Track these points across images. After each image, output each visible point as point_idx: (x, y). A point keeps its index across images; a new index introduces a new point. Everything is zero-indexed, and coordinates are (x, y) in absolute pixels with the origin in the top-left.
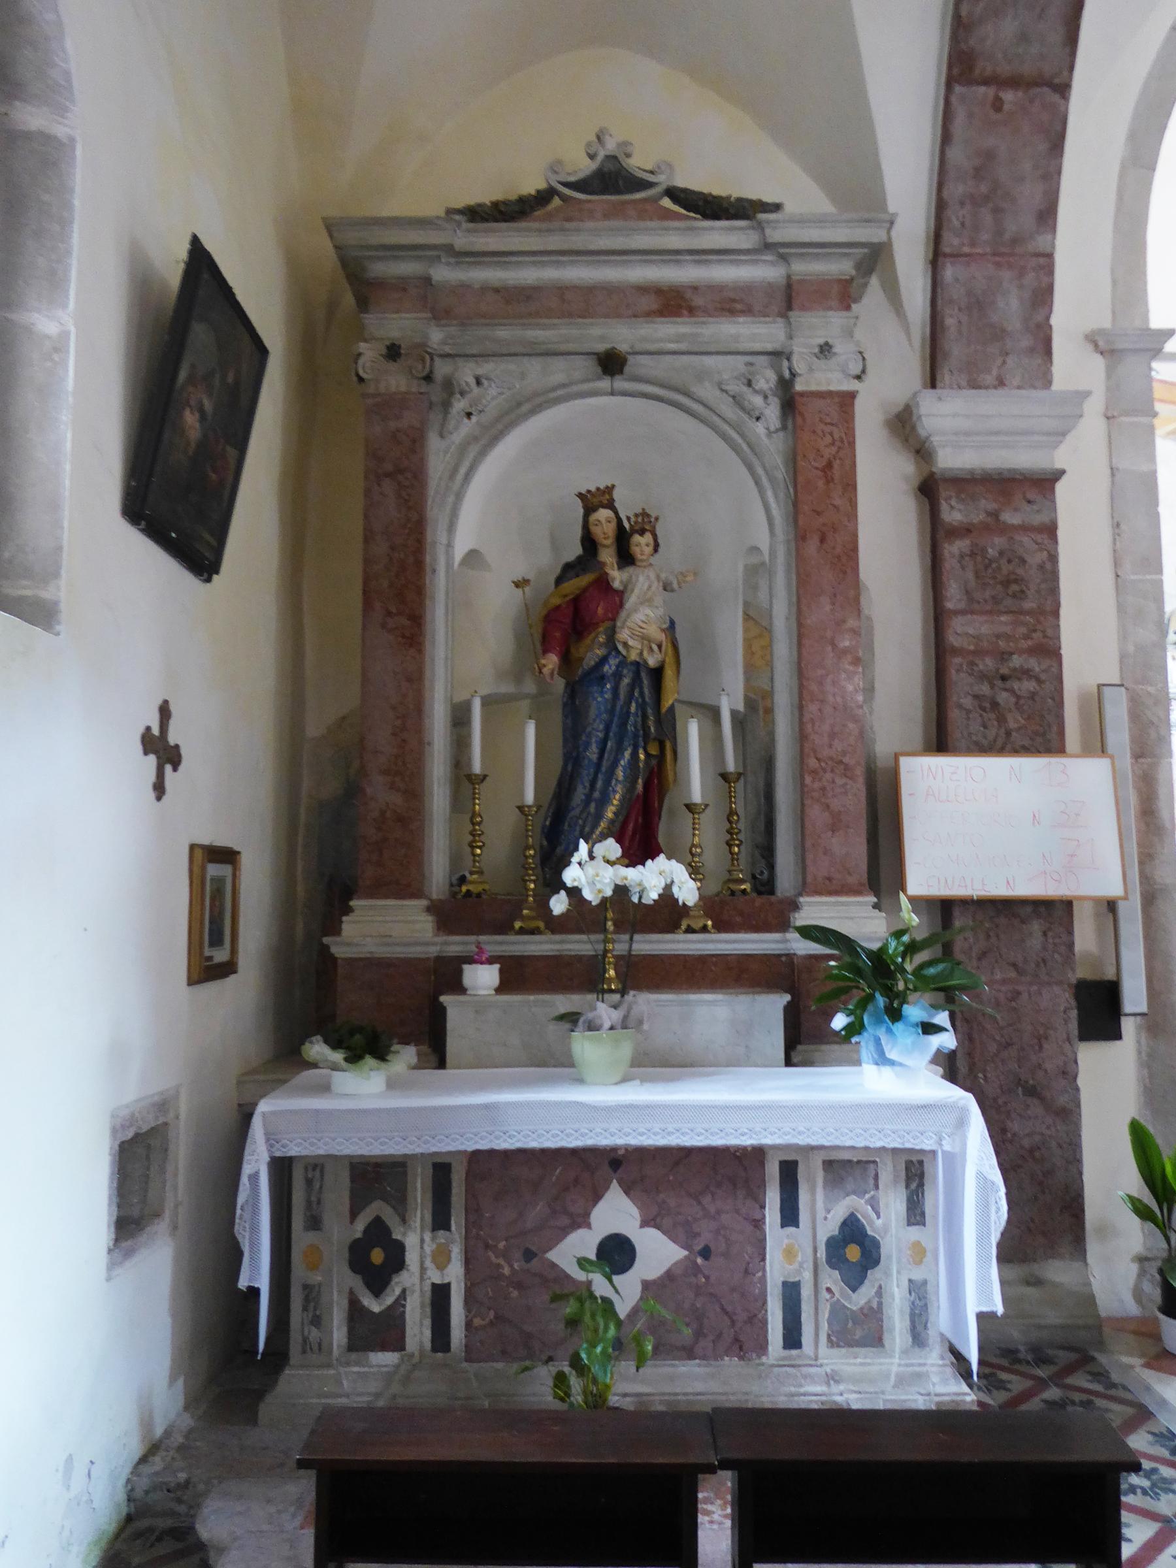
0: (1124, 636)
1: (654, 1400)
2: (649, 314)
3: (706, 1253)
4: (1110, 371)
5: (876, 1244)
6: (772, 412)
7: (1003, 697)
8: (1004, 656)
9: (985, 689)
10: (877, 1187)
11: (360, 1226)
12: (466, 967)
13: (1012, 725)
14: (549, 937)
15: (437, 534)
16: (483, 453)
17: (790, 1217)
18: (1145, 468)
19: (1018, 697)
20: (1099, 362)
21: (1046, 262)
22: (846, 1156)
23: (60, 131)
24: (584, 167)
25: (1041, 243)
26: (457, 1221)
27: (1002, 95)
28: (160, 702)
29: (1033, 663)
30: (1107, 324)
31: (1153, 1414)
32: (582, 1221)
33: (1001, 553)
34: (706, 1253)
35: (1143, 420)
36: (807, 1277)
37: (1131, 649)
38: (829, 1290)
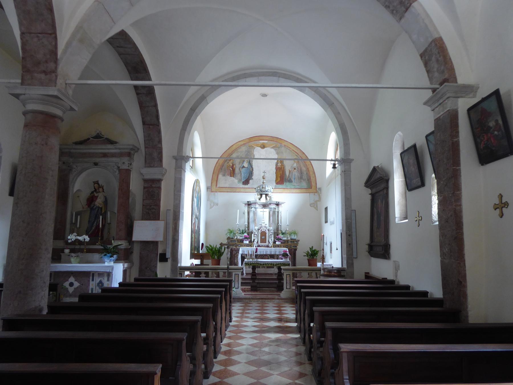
0: (174, 202)
2: (102, 157)
3: (82, 284)
4: (176, 162)
5: (103, 284)
6: (117, 172)
8: (151, 206)
9: (147, 211)
10: (104, 277)
12: (65, 250)
13: (151, 216)
17: (93, 280)
18: (180, 177)
19: (152, 212)
20: (174, 161)
21: (161, 149)
22: (101, 273)
24: (94, 134)
25: (159, 145)
27: (150, 126)
30: (176, 155)
31: (253, 351)
32: (68, 280)
34: (82, 284)
36: (94, 288)
37: (175, 204)
38: (97, 289)
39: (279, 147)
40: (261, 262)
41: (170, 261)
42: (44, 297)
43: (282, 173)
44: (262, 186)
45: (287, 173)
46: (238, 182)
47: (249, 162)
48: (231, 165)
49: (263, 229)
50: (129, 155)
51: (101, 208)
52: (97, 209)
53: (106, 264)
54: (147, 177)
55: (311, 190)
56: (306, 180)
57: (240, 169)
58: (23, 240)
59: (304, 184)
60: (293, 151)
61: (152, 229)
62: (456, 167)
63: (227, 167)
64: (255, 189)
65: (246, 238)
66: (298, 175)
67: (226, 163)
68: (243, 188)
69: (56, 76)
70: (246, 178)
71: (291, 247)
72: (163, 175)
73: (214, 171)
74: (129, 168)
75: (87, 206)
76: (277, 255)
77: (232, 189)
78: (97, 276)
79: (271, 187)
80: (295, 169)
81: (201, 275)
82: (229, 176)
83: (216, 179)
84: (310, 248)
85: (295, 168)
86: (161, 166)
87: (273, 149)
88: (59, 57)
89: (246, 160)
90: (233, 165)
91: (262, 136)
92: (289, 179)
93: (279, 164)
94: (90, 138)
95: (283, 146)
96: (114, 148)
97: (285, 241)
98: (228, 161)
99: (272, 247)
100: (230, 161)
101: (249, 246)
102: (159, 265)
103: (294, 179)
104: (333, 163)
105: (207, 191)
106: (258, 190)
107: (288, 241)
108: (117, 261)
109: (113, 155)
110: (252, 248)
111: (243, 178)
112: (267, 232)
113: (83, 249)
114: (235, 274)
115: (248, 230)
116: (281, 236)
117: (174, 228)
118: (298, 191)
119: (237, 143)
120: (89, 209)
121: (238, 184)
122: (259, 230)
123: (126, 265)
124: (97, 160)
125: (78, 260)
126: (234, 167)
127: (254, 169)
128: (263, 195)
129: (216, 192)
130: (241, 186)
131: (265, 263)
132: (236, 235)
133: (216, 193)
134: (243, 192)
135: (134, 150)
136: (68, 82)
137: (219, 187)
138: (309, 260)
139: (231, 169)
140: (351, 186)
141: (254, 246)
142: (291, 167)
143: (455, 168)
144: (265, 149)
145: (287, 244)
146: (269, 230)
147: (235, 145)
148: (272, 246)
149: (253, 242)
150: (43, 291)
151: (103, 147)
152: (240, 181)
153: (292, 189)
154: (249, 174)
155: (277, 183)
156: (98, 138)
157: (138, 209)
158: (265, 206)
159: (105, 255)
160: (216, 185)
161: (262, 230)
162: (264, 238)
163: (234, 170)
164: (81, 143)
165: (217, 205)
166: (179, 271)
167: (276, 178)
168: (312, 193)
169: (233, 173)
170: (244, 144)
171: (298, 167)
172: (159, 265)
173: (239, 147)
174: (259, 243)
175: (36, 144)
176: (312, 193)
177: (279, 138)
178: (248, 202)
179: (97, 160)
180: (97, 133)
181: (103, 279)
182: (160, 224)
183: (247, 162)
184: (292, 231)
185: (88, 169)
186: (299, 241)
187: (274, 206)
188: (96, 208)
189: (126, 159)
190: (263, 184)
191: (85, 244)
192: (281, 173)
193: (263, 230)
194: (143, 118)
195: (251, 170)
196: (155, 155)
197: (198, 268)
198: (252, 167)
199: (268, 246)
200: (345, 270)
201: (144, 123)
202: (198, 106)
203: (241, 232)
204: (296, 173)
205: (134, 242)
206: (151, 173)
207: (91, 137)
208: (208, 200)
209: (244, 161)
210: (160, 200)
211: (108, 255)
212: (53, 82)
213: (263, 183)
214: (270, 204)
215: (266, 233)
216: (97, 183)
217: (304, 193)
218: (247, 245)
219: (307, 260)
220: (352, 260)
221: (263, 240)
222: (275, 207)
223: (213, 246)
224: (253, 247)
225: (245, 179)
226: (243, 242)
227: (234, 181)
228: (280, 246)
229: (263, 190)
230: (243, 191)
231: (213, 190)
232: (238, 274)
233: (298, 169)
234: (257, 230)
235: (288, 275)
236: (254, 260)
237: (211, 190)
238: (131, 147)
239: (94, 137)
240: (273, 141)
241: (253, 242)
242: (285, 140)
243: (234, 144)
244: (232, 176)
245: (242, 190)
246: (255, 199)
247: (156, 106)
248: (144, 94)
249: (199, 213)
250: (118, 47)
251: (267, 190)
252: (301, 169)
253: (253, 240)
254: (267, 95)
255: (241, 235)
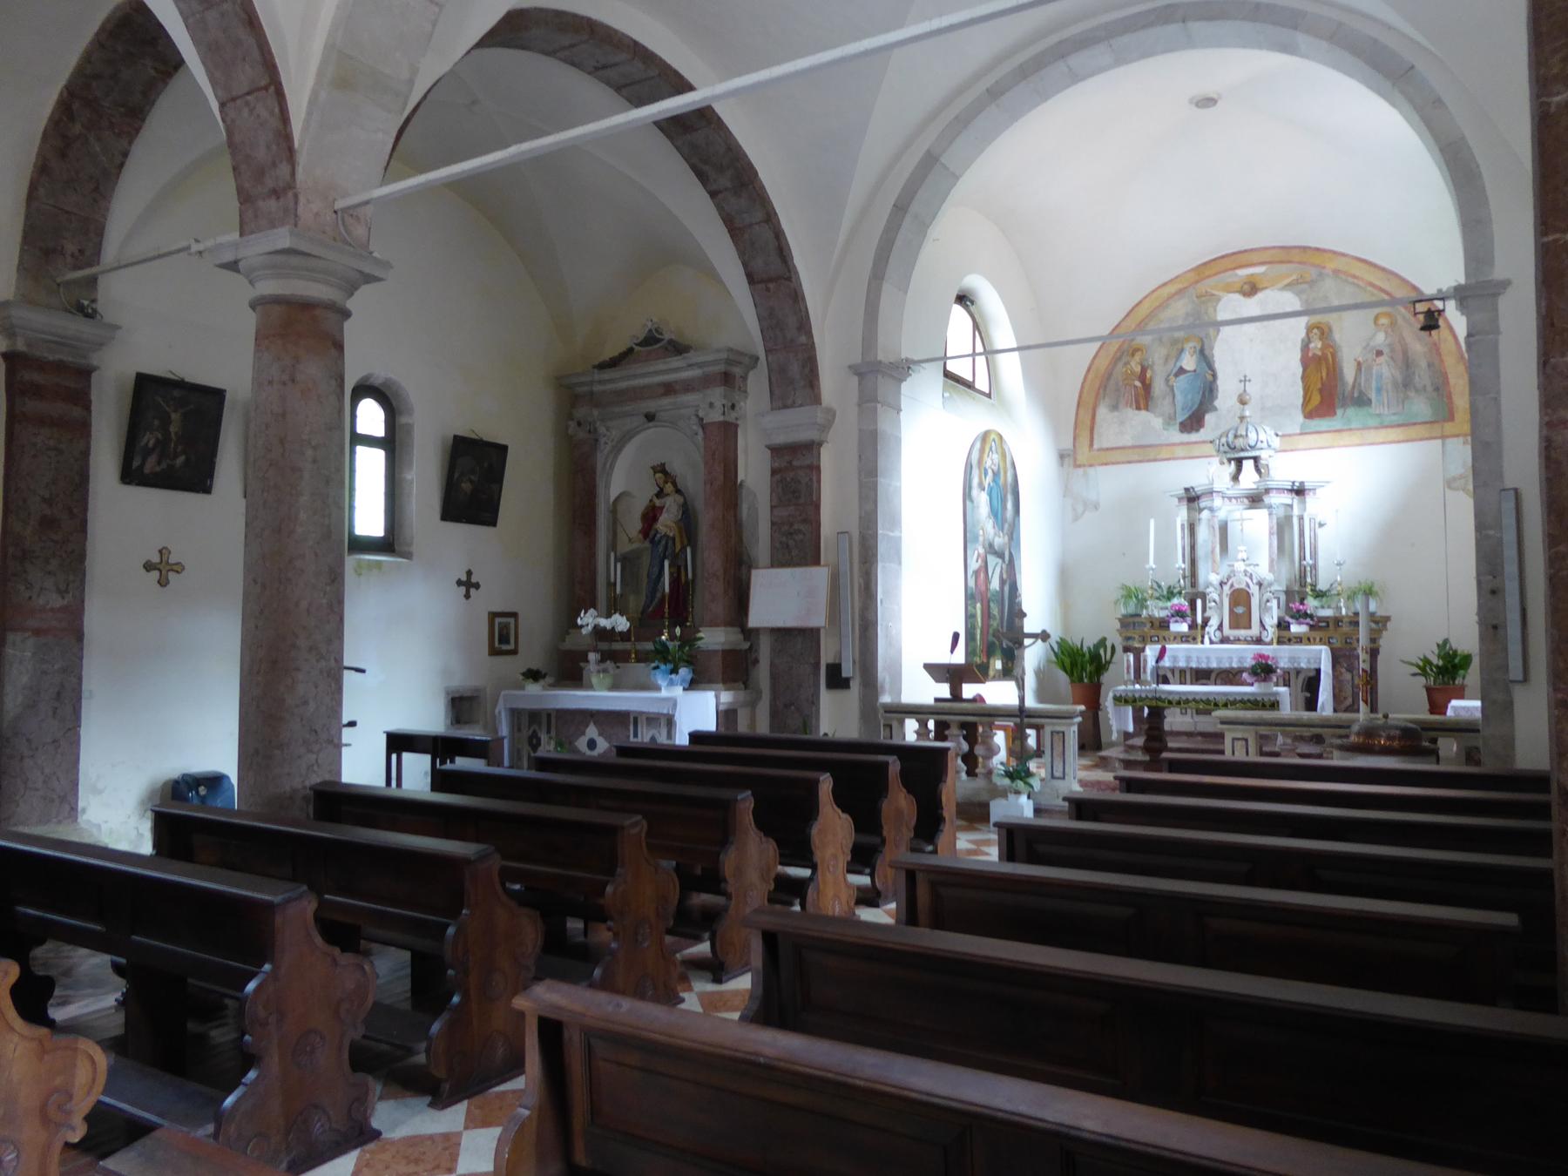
1: (529, 768)
6: (700, 432)
7: (791, 542)
8: (791, 525)
9: (784, 539)
11: (531, 732)
14: (620, 643)
15: (601, 491)
16: (616, 458)
20: (856, 379)
23: (410, 421)
26: (553, 733)
28: (467, 569)
29: (802, 527)
33: (792, 479)
35: (873, 404)
39: (1312, 281)
40: (1170, 693)
41: (855, 685)
42: (315, 768)
43: (1328, 374)
44: (1236, 430)
45: (1349, 373)
46: (1163, 424)
47: (1202, 352)
48: (1138, 369)
49: (1240, 582)
50: (727, 379)
51: (674, 539)
52: (663, 542)
53: (664, 693)
54: (780, 439)
55: (1449, 427)
56: (1429, 388)
57: (1167, 380)
58: (257, 627)
59: (1421, 407)
60: (1369, 288)
61: (798, 593)
62: (1557, 236)
63: (1125, 379)
64: (1211, 442)
65: (1179, 614)
66: (1392, 374)
67: (1120, 365)
68: (1182, 444)
69: (296, 196)
70: (1191, 408)
71: (1350, 643)
72: (826, 427)
73: (1080, 397)
74: (731, 417)
75: (641, 536)
76: (1180, 672)
77: (1144, 452)
78: (645, 728)
79: (1268, 432)
80: (1379, 353)
81: (947, 732)
82: (1131, 406)
83: (1089, 423)
84: (1438, 645)
85: (1378, 348)
86: (816, 399)
87: (1290, 290)
88: (296, 144)
89: (1189, 346)
90: (1144, 370)
91: (1246, 251)
92: (1356, 395)
93: (1316, 345)
94: (634, 346)
95: (1331, 273)
96: (685, 365)
97: (1328, 623)
98: (1124, 359)
99: (1272, 644)
100: (1133, 355)
101: (1190, 639)
102: (826, 698)
103: (1379, 390)
104: (1426, 309)
105: (1062, 465)
106: (1222, 448)
107: (1337, 621)
108: (693, 685)
109: (688, 386)
110: (1200, 646)
111: (1183, 409)
112: (1254, 589)
113: (628, 653)
114: (1052, 733)
115: (1194, 584)
116: (1311, 604)
117: (863, 585)
118: (1393, 434)
119: (1154, 291)
120: (647, 544)
121: (1165, 432)
122: (1226, 583)
123: (727, 697)
124: (651, 406)
125: (608, 681)
126: (1148, 376)
127: (1220, 375)
128: (1244, 462)
129: (1091, 466)
130: (1177, 436)
131: (1184, 698)
132: (1148, 603)
133: (1091, 471)
134: (1184, 458)
135: (740, 363)
136: (339, 205)
137: (1099, 450)
138: (1429, 690)
139: (1138, 384)
140: (1498, 392)
141: (1206, 639)
142: (1365, 348)
143: (1556, 241)
144: (1260, 296)
145: (1336, 630)
146: (1260, 584)
147: (1147, 299)
148: (1272, 639)
149: (1199, 627)
150: (310, 751)
151: (660, 366)
152: (1169, 420)
153: (1369, 428)
154: (1204, 393)
155: (1309, 415)
156: (651, 345)
157: (761, 538)
158: (1255, 500)
159: (657, 668)
160: (1091, 445)
161: (1235, 584)
162: (1243, 613)
163: (1147, 387)
164: (613, 363)
165: (1096, 507)
166: (885, 719)
167: (1305, 397)
168: (1456, 439)
169: (1143, 397)
170: (1180, 292)
171: (1390, 345)
172: (826, 698)
173: (1163, 305)
174: (1227, 631)
175: (270, 383)
176: (1457, 436)
177: (1310, 248)
178: (1187, 490)
179: (651, 406)
180: (647, 330)
181: (659, 732)
182: (819, 576)
183: (1195, 352)
184: (1360, 583)
185: (638, 432)
186: (1387, 619)
187: (1287, 499)
188: (660, 541)
189: (717, 395)
190: (1241, 421)
191: (633, 639)
192: (1324, 375)
193: (1240, 583)
194: (745, 265)
195: (1210, 378)
196: (795, 369)
197: (943, 708)
198: (1211, 367)
199: (1259, 641)
200: (1478, 731)
201: (751, 278)
202: (916, 192)
203: (1165, 593)
204: (1385, 370)
205: (757, 631)
206: (792, 425)
207: (637, 345)
208: (1064, 496)
209: (1182, 351)
210: (817, 507)
211: (663, 667)
212: (290, 215)
213: (1242, 418)
214: (1267, 491)
215: (1248, 596)
216: (661, 469)
217: (1421, 439)
218: (1184, 638)
219: (1424, 690)
220: (1508, 692)
221: (1240, 620)
222: (1289, 501)
223: (1070, 642)
224: (1202, 642)
225: (1190, 413)
226: (1168, 627)
227: (1150, 424)
228: (1305, 640)
229: (1240, 442)
230: (1181, 455)
231: (1081, 459)
232: (1063, 733)
233: (1393, 350)
234: (1219, 587)
235: (1240, 742)
236: (1148, 687)
237: (1075, 460)
238: (724, 355)
239: (641, 342)
240: (1290, 262)
241: (1199, 627)
242: (1334, 253)
243: (1146, 297)
244: (1142, 406)
245: (1180, 451)
246: (1208, 477)
247: (771, 218)
248: (726, 189)
249: (1011, 538)
250: (597, 69)
251: (1252, 444)
252: (1405, 353)
253: (1199, 620)
254: (1215, 96)
255: (1161, 604)
